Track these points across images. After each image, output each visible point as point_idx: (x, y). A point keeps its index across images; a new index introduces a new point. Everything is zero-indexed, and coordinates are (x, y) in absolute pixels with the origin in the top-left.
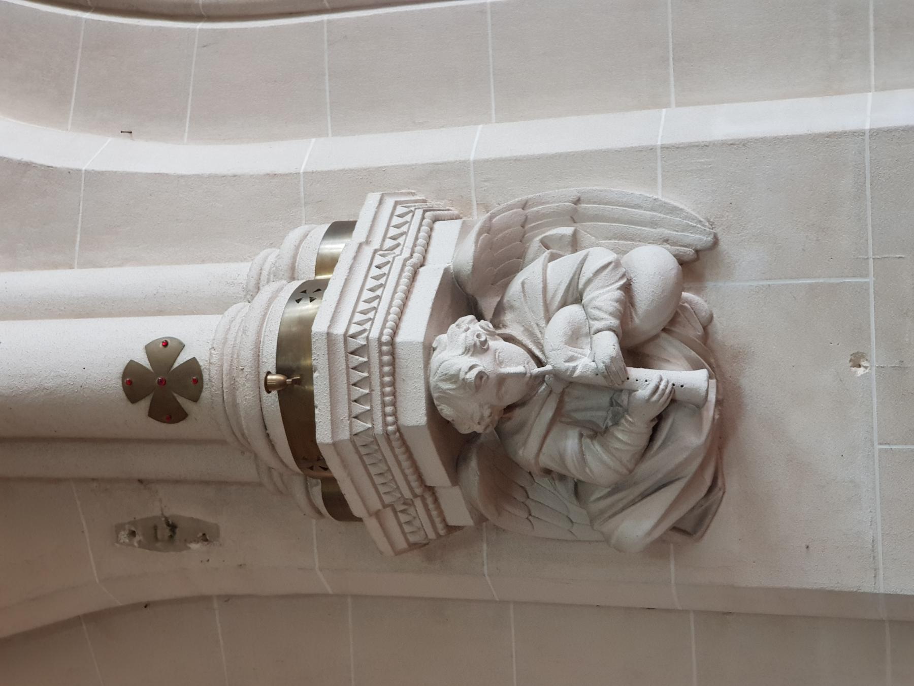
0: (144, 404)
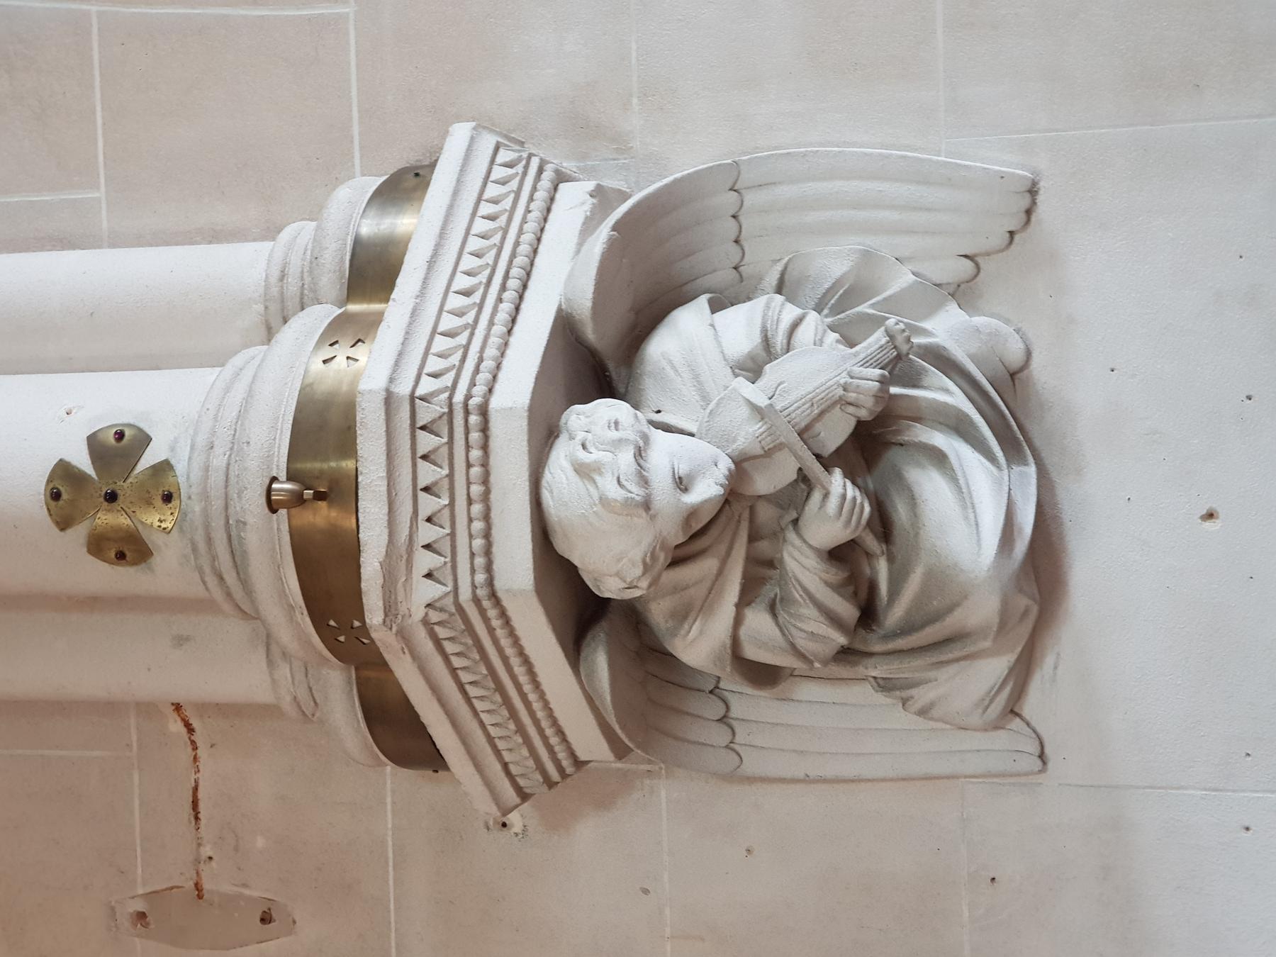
0: (82, 461)
